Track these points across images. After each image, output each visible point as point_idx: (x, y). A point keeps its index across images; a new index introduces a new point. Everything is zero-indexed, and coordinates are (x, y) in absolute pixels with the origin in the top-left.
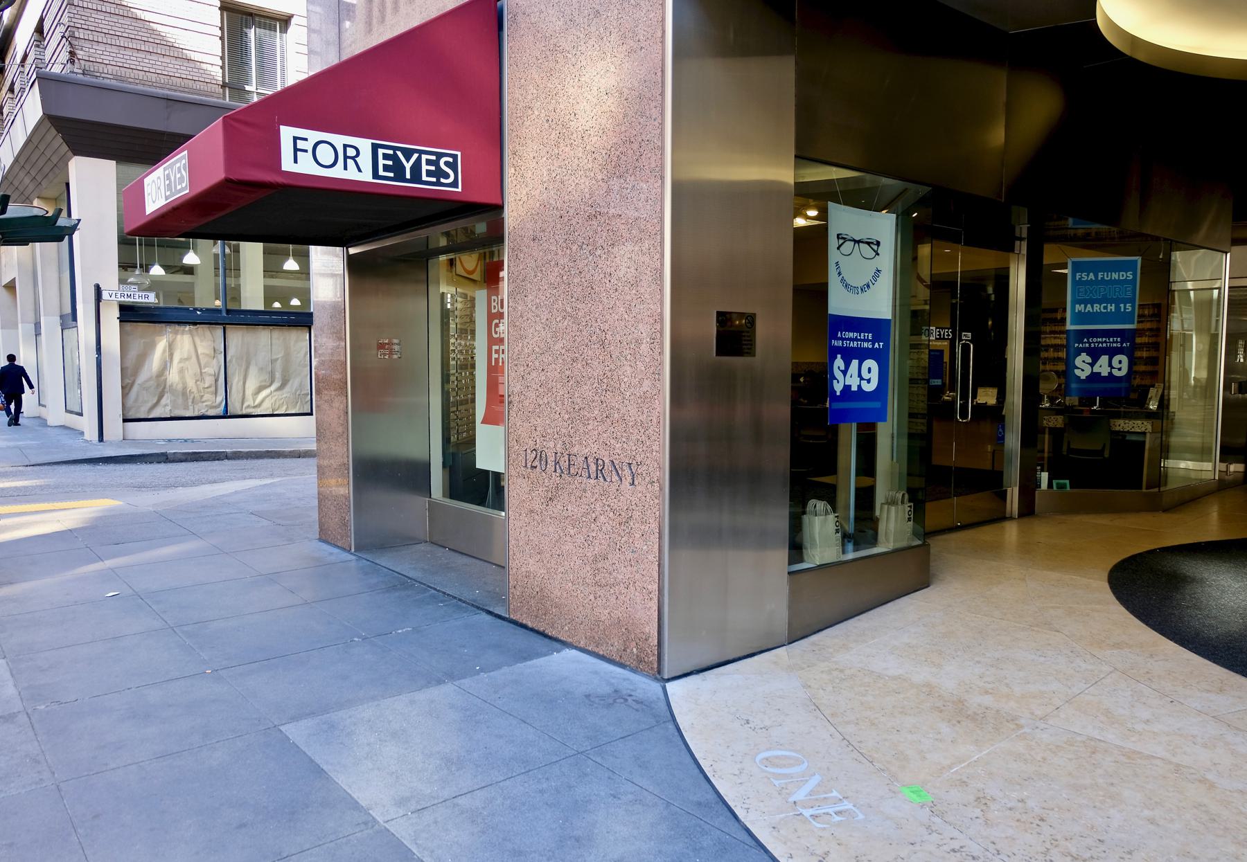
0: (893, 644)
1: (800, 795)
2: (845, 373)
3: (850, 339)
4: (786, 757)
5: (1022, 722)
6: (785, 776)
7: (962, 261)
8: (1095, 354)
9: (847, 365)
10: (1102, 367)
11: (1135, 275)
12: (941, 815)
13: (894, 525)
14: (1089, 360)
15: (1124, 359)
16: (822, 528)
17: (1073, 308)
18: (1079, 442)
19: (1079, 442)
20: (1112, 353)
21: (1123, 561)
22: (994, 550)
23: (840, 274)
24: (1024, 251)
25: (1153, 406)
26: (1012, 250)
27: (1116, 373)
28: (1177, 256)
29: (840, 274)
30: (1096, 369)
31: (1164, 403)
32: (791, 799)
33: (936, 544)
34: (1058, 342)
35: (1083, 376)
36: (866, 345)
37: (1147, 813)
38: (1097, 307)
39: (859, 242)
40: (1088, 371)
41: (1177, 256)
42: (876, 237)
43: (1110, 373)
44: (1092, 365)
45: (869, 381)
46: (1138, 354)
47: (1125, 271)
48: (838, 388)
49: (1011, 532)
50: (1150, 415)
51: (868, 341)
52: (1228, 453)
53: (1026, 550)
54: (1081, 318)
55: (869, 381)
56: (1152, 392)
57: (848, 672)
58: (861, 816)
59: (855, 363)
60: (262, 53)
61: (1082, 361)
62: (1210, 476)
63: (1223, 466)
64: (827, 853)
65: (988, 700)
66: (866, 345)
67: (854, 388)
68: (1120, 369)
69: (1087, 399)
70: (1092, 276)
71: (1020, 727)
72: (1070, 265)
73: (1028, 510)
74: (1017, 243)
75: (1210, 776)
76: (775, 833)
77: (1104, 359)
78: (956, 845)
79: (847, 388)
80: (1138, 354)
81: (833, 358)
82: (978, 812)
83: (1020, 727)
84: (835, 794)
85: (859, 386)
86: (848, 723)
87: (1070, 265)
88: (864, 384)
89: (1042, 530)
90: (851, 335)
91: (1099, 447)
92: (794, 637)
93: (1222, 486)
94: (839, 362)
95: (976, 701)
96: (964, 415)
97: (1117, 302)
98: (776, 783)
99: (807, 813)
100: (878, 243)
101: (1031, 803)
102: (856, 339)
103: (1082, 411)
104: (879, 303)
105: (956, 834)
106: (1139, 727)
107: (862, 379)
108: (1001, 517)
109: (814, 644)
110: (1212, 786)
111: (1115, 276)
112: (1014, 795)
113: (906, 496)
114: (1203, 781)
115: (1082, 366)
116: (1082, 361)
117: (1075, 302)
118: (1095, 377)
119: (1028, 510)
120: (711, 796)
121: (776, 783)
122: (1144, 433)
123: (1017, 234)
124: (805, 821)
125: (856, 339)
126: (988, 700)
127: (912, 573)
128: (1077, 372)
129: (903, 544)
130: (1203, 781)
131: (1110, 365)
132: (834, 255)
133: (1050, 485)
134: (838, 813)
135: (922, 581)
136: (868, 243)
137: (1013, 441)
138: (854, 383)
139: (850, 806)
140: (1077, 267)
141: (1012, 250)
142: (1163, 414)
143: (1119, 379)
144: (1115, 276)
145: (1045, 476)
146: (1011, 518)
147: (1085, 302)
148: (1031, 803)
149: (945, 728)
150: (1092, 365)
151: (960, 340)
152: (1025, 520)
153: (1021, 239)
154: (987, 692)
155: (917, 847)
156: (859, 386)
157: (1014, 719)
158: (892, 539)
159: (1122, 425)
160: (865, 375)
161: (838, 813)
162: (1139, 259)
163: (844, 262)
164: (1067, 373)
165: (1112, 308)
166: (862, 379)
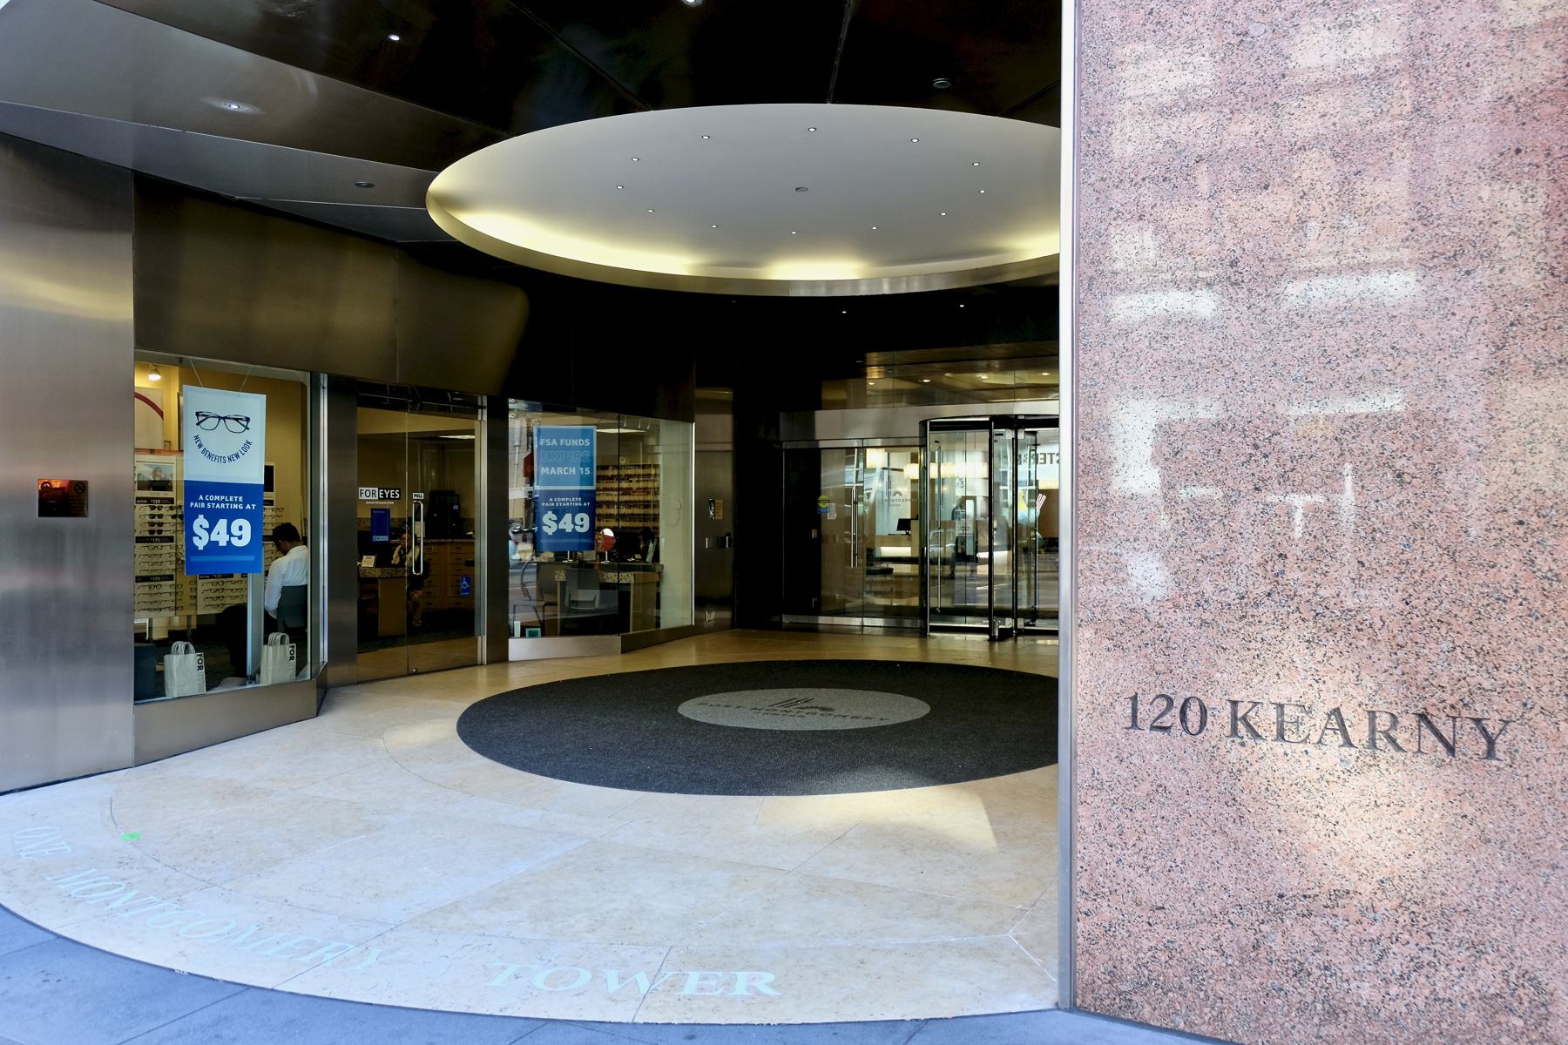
3: (216, 501)
8: (559, 513)
14: (206, 524)
15: (586, 517)
20: (231, 516)
27: (578, 529)
30: (561, 526)
34: (609, 498)
38: (560, 470)
40: (554, 527)
43: (229, 542)
44: (557, 522)
46: (599, 511)
55: (240, 538)
60: (399, 390)
68: (240, 538)
80: (599, 511)
96: (418, 570)
100: (248, 420)
107: (231, 535)
108: (474, 664)
120: (52, 937)
131: (229, 532)
143: (581, 535)
150: (557, 522)
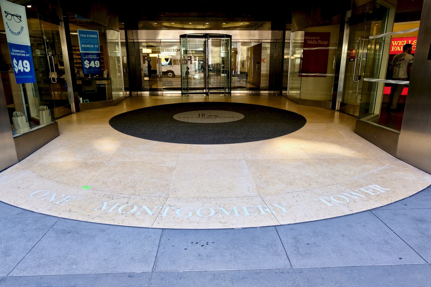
0: (59, 154)
1: (52, 199)
2: (17, 65)
4: (42, 192)
5: (105, 163)
6: (43, 197)
7: (46, 27)
8: (76, 60)
9: (18, 62)
10: (92, 64)
11: (97, 36)
12: (96, 189)
13: (45, 118)
14: (88, 62)
16: (21, 122)
17: (81, 46)
18: (87, 88)
19: (87, 88)
21: (112, 118)
22: (70, 122)
23: (8, 27)
24: (63, 25)
25: (105, 76)
26: (59, 24)
27: (96, 66)
28: (108, 31)
29: (8, 27)
30: (91, 65)
31: (108, 75)
32: (50, 201)
33: (60, 122)
35: (87, 67)
36: (23, 55)
37: (141, 173)
39: (13, 15)
41: (108, 31)
42: (19, 14)
44: (89, 64)
45: (27, 68)
47: (95, 35)
48: (17, 71)
49: (74, 117)
50: (104, 79)
51: (23, 53)
52: (126, 89)
53: (79, 122)
54: (84, 49)
55: (27, 68)
56: (104, 72)
57: (46, 165)
58: (74, 198)
59: (20, 61)
61: (86, 62)
62: (121, 96)
63: (125, 93)
64: (70, 209)
65: (93, 161)
66: (23, 55)
67: (22, 71)
69: (86, 76)
70: (85, 36)
71: (105, 164)
72: (78, 31)
73: (78, 110)
74: (60, 22)
75: (150, 162)
76: (51, 211)
77: (93, 62)
78: (103, 194)
79: (19, 71)
81: (13, 60)
82: (105, 186)
83: (105, 164)
84: (63, 195)
85: (24, 70)
86: (55, 177)
87: (78, 31)
88: (25, 69)
89: (83, 115)
90: (17, 51)
91: (93, 89)
92: (21, 158)
93: (125, 98)
94: (15, 61)
95: (90, 161)
97: (94, 44)
98: (42, 199)
99: (58, 203)
101: (116, 180)
102: (19, 53)
103: (86, 79)
104: (25, 40)
105: (102, 192)
106: (132, 156)
107: (24, 67)
108: (71, 113)
109: (28, 160)
110: (151, 163)
111: (92, 36)
112: (111, 179)
113: (47, 107)
114: (149, 163)
115: (87, 64)
116: (86, 62)
117: (81, 44)
118: (90, 67)
119: (78, 110)
121: (42, 199)
122: (105, 84)
123: (60, 19)
124: (58, 205)
125: (19, 53)
126: (93, 161)
127: (53, 132)
128: (85, 66)
129: (49, 123)
130: (149, 163)
132: (5, 20)
133: (83, 102)
134: (67, 199)
135: (57, 134)
136: (17, 16)
137: (70, 89)
138: (22, 69)
139: (70, 197)
140: (80, 32)
141: (59, 24)
142: (108, 78)
144: (92, 36)
145: (81, 99)
146: (74, 113)
147: (85, 44)
148: (116, 180)
149: (85, 170)
151: (48, 55)
152: (78, 113)
153: (62, 21)
154: (92, 159)
155: (94, 198)
156: (24, 70)
157: (102, 163)
158: (45, 122)
159: (98, 82)
160: (96, 64)
161: (67, 199)
162: (98, 31)
163: (9, 22)
164: (82, 67)
165: (92, 46)
166: (24, 67)
